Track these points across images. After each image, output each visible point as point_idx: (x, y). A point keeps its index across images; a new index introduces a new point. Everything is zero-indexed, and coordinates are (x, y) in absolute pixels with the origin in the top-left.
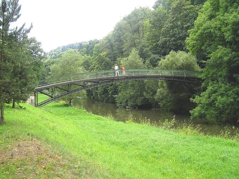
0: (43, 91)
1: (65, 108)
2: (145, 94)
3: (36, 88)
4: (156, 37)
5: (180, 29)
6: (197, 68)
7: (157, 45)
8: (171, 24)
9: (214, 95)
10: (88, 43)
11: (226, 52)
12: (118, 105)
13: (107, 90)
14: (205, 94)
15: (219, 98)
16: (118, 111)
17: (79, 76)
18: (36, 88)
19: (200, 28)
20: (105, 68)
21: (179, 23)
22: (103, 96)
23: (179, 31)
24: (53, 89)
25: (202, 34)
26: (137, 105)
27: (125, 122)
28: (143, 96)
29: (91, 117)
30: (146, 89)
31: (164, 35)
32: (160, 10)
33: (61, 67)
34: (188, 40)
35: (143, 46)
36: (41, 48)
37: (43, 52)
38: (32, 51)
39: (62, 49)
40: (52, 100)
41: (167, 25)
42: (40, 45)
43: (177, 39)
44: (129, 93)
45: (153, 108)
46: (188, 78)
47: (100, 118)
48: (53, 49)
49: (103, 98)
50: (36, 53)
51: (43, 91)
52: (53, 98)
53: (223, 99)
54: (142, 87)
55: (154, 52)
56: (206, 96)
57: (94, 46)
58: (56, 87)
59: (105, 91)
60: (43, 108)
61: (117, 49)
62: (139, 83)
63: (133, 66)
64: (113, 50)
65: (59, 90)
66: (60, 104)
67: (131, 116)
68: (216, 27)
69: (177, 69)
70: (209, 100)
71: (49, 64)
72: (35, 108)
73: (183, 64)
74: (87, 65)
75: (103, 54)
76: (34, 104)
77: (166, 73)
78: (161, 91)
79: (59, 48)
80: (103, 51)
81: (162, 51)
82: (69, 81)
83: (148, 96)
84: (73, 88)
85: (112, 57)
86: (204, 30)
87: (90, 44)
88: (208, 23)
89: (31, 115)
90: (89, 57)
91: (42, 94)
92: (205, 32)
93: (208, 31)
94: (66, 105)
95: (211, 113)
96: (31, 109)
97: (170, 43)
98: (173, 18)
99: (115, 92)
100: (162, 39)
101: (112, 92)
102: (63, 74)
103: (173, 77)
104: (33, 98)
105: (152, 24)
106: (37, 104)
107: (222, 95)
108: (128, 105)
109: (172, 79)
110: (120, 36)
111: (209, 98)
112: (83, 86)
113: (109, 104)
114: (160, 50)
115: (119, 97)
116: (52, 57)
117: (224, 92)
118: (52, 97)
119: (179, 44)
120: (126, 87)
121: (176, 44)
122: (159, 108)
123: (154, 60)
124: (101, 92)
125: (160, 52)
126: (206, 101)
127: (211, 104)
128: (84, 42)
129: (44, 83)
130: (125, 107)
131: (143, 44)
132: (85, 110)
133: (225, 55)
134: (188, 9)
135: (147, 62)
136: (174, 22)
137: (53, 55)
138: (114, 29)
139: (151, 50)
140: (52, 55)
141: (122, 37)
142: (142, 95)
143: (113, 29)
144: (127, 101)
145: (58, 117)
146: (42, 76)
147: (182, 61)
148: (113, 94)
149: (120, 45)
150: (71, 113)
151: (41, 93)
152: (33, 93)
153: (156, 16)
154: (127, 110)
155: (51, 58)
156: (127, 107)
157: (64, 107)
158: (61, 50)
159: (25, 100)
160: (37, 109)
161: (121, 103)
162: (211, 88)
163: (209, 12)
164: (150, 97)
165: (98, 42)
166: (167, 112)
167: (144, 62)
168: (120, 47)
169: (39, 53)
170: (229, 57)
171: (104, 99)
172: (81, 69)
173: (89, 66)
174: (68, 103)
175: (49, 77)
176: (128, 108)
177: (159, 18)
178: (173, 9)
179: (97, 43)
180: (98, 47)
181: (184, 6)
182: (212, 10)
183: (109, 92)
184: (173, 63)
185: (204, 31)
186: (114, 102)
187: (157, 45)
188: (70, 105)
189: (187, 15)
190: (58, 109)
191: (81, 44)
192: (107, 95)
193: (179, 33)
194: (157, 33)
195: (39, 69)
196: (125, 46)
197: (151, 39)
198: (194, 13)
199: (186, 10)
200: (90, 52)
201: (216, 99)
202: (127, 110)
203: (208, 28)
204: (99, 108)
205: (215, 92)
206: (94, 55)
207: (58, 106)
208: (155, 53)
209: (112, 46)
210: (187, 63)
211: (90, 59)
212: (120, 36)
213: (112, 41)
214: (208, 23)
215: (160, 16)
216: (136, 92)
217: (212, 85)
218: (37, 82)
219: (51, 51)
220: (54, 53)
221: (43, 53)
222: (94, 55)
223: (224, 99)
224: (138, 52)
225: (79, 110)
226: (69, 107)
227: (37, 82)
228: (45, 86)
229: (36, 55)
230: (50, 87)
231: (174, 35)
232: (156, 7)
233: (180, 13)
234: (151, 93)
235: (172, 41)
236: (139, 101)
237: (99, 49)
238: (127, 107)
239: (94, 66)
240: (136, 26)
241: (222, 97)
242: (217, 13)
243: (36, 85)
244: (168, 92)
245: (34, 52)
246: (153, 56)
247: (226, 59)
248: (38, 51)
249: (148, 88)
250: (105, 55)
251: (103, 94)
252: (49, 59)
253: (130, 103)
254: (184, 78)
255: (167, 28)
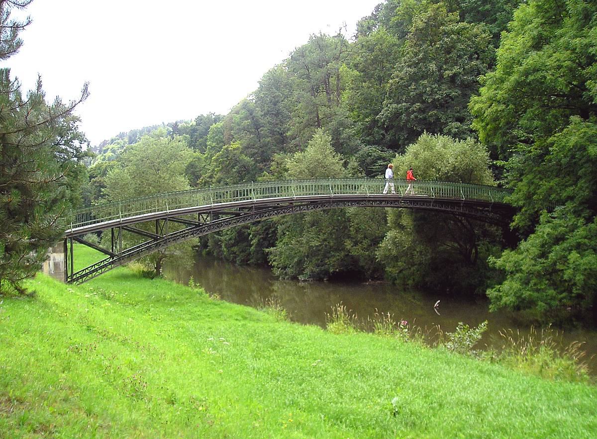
0: (85, 238)
1: (147, 283)
2: (348, 244)
4: (370, 104)
5: (435, 81)
6: (488, 178)
7: (375, 122)
8: (412, 70)
9: (558, 247)
10: (195, 123)
12: (277, 272)
14: (530, 245)
15: (574, 256)
16: (276, 286)
17: (180, 197)
20: (240, 180)
21: (433, 66)
22: (235, 249)
24: (116, 234)
25: (519, 84)
26: (326, 272)
27: (324, 327)
28: (343, 249)
29: (225, 311)
30: (353, 233)
31: (398, 94)
32: (382, 37)
35: (341, 124)
36: (80, 130)
37: (85, 141)
39: (130, 138)
40: (112, 263)
41: (401, 71)
42: (77, 123)
44: (307, 243)
45: (366, 280)
46: (470, 205)
47: (249, 313)
48: (109, 138)
49: (235, 253)
50: (66, 143)
51: (85, 238)
52: (118, 259)
53: (585, 260)
54: (342, 228)
55: (368, 138)
56: (535, 251)
58: (121, 227)
59: (241, 237)
61: (270, 133)
63: (316, 172)
64: (259, 136)
66: (131, 272)
68: (559, 67)
69: (440, 179)
70: (544, 263)
71: (99, 171)
72: (64, 286)
73: (455, 167)
75: (236, 145)
76: (63, 276)
77: (410, 190)
78: (396, 238)
79: (121, 136)
80: (234, 140)
81: (388, 137)
82: (158, 210)
83: (356, 251)
84: (169, 230)
85: (257, 153)
86: (527, 73)
88: (533, 58)
89: (53, 327)
90: (198, 154)
92: (531, 78)
93: (538, 75)
95: (549, 297)
96: (53, 292)
97: (408, 115)
98: (416, 54)
100: (388, 109)
101: (259, 241)
102: (139, 193)
103: (434, 202)
104: (59, 257)
105: (360, 71)
106: (72, 275)
108: (303, 274)
109: (431, 207)
110: (277, 102)
111: (543, 255)
114: (383, 135)
115: (278, 253)
117: (586, 241)
118: (112, 256)
120: (298, 227)
121: (425, 119)
122: (383, 279)
123: (369, 160)
124: (230, 239)
127: (551, 275)
130: (295, 278)
132: (202, 290)
134: (453, 32)
135: (354, 163)
136: (418, 63)
137: (109, 151)
138: (258, 86)
139: (358, 133)
140: (105, 151)
141: (281, 105)
142: (339, 247)
143: (256, 87)
144: (300, 263)
145: (131, 311)
148: (260, 245)
149: (277, 124)
150: (165, 299)
151: (81, 242)
152: (58, 245)
153: (372, 50)
154: (301, 284)
155: (104, 159)
156: (301, 278)
158: (126, 140)
159: (33, 269)
160: (71, 289)
161: (285, 268)
162: (548, 230)
163: (533, 29)
166: (405, 290)
167: (345, 165)
168: (276, 129)
169: (76, 143)
171: (236, 257)
172: (183, 183)
173: (198, 177)
174: (152, 268)
175: (103, 201)
176: (305, 281)
178: (416, 30)
179: (215, 121)
181: (442, 24)
182: (542, 24)
183: (252, 240)
184: (429, 165)
185: (527, 77)
186: (264, 264)
187: (375, 122)
188: (158, 273)
189: (452, 47)
190: (128, 284)
193: (433, 92)
197: (358, 108)
198: (469, 43)
199: (447, 34)
201: (564, 259)
202: (301, 284)
203: (536, 70)
204: (225, 278)
205: (559, 239)
207: (125, 277)
208: (369, 143)
209: (257, 126)
211: (199, 159)
213: (258, 113)
214: (533, 58)
215: (380, 50)
216: (325, 240)
218: (72, 214)
219: (105, 143)
220: (110, 147)
221: (86, 143)
222: (210, 149)
224: (330, 138)
225: (184, 288)
226: (157, 281)
227: (72, 214)
228: (90, 226)
229: (69, 149)
230: (107, 226)
231: (419, 97)
234: (366, 242)
235: (414, 112)
236: (333, 264)
237: (221, 136)
238: (301, 278)
239: (211, 177)
240: (319, 74)
242: (558, 32)
244: (414, 241)
245: (63, 142)
246: (365, 149)
248: (74, 138)
249: (357, 230)
251: (233, 245)
252: (99, 160)
253: (309, 268)
254: (460, 203)
255: (402, 79)
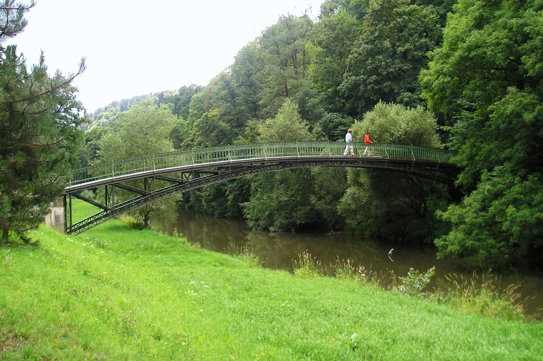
0: (82, 194)
2: (313, 199)
3: (68, 187)
6: (436, 141)
7: (336, 92)
8: (369, 47)
9: (497, 202)
10: (178, 93)
11: (525, 102)
12: (251, 224)
13: (224, 190)
15: (511, 209)
18: (68, 187)
19: (460, 46)
21: (387, 43)
22: (214, 203)
23: (388, 61)
24: (109, 191)
25: (463, 59)
26: (294, 224)
27: (292, 272)
29: (204, 258)
31: (359, 63)
32: (342, 18)
33: (125, 139)
34: (425, 75)
35: (307, 94)
36: (77, 99)
37: (82, 109)
38: (59, 106)
39: (122, 106)
40: (106, 216)
42: (75, 93)
43: (382, 79)
44: (277, 198)
45: (329, 231)
46: (419, 164)
47: (226, 260)
48: (103, 107)
50: (66, 111)
51: (82, 194)
53: (520, 213)
55: (330, 107)
56: (477, 205)
57: (191, 97)
58: (114, 184)
59: (219, 193)
60: (85, 235)
61: (245, 102)
62: (299, 174)
64: (234, 105)
65: (120, 191)
66: (123, 224)
67: (306, 256)
68: (498, 44)
69: (393, 142)
70: (484, 216)
71: (94, 135)
73: (407, 131)
74: (177, 137)
75: (214, 112)
76: (63, 227)
77: (367, 152)
79: (114, 104)
81: (348, 106)
83: (320, 206)
84: (155, 187)
85: (233, 119)
86: (469, 49)
87: (181, 94)
88: (475, 36)
90: (181, 120)
91: (80, 200)
92: (473, 53)
93: (480, 51)
94: (137, 227)
95: (489, 246)
96: (54, 242)
97: (366, 86)
98: (372, 33)
99: (239, 195)
102: (130, 154)
104: (59, 211)
105: (323, 48)
106: (71, 226)
107: (515, 202)
108: (273, 225)
109: (386, 167)
110: (251, 74)
111: (484, 209)
112: (180, 183)
113: (226, 221)
114: (343, 103)
116: (100, 123)
117: (522, 196)
118: (106, 209)
119: (386, 91)
121: (380, 89)
122: (343, 230)
123: (331, 125)
124: (209, 195)
125: (343, 107)
126: (476, 218)
128: (166, 92)
129: (85, 176)
130: (266, 229)
131: (305, 89)
133: (525, 108)
134: (405, 13)
135: (318, 128)
136: (374, 41)
137: (103, 118)
138: (234, 60)
142: (305, 202)
143: (232, 61)
144: (270, 216)
145: (122, 258)
146: (80, 161)
147: (403, 126)
148: (235, 200)
149: (250, 94)
151: (79, 197)
152: (59, 200)
153: (334, 29)
154: (272, 234)
155: (99, 125)
157: (134, 230)
158: (118, 108)
160: (70, 239)
161: (257, 220)
164: (326, 206)
165: (198, 90)
169: (74, 111)
170: (535, 113)
171: (214, 211)
172: (168, 146)
173: (181, 140)
174: (142, 221)
175: (98, 161)
176: (275, 232)
177: (338, 35)
178: (373, 12)
180: (200, 101)
181: (396, 7)
183: (228, 195)
184: (384, 130)
185: (470, 53)
187: (336, 92)
191: (161, 96)
192: (224, 201)
194: (335, 66)
195: (73, 145)
196: (263, 97)
197: (322, 79)
198: (419, 23)
199: (400, 15)
200: (181, 111)
201: (502, 213)
202: (272, 234)
203: (478, 47)
204: (205, 229)
205: (498, 195)
206: (191, 116)
207: (117, 228)
208: (331, 111)
209: (233, 95)
210: (417, 130)
211: (182, 125)
212: (251, 74)
214: (475, 36)
215: (341, 29)
217: (489, 180)
218: (70, 173)
219: (99, 111)
220: (105, 114)
221: (83, 111)
223: (525, 212)
225: (169, 238)
226: (145, 232)
227: (70, 173)
229: (68, 116)
231: (375, 71)
232: (327, 11)
233: (387, 22)
234: (328, 198)
235: (370, 83)
236: (299, 216)
237: (202, 105)
239: (192, 140)
241: (518, 210)
242: (497, 13)
243: (68, 181)
244: (370, 197)
245: (63, 110)
246: (328, 116)
247: (528, 117)
248: (72, 106)
249: (321, 187)
250: (216, 116)
251: (212, 200)
252: (94, 126)
255: (360, 54)
